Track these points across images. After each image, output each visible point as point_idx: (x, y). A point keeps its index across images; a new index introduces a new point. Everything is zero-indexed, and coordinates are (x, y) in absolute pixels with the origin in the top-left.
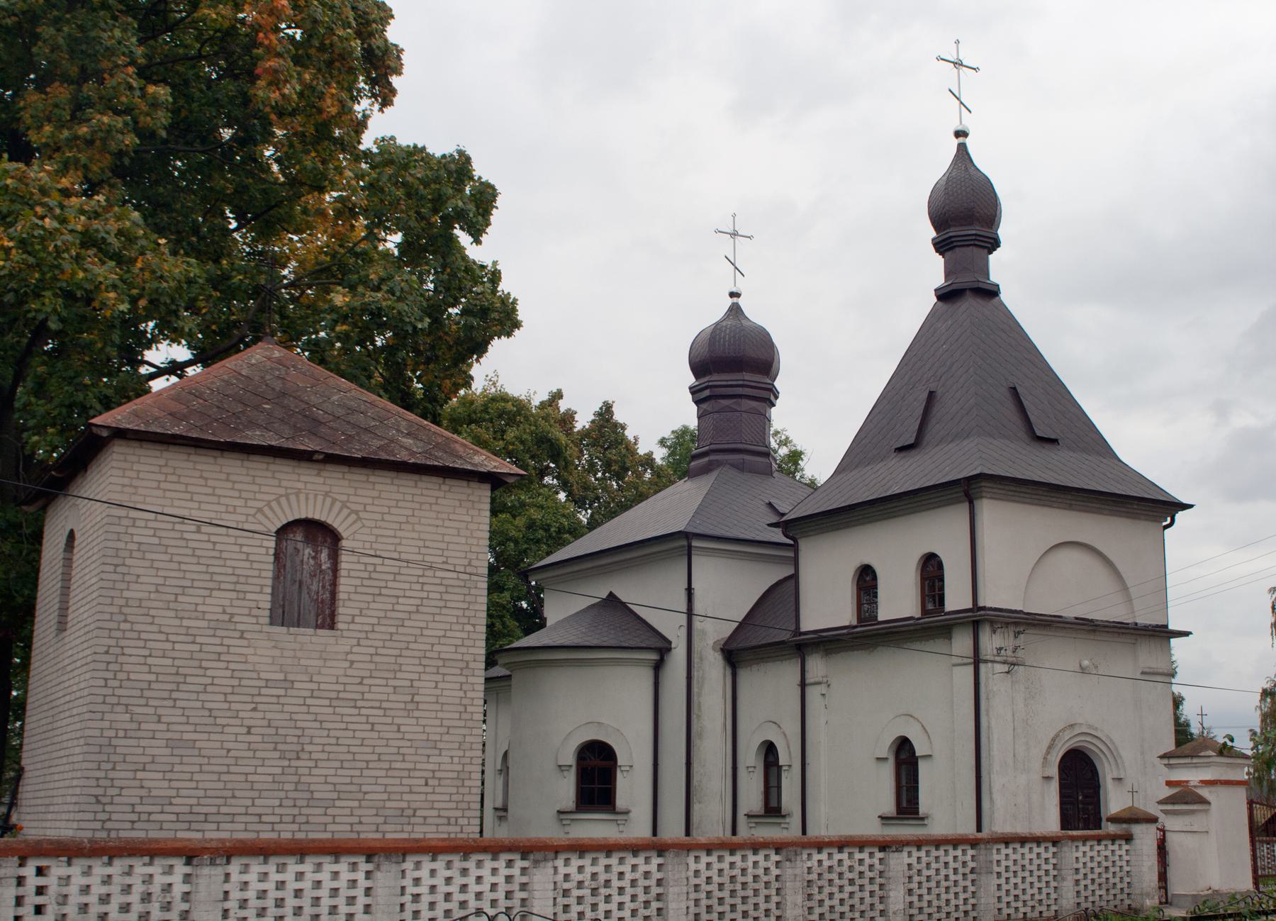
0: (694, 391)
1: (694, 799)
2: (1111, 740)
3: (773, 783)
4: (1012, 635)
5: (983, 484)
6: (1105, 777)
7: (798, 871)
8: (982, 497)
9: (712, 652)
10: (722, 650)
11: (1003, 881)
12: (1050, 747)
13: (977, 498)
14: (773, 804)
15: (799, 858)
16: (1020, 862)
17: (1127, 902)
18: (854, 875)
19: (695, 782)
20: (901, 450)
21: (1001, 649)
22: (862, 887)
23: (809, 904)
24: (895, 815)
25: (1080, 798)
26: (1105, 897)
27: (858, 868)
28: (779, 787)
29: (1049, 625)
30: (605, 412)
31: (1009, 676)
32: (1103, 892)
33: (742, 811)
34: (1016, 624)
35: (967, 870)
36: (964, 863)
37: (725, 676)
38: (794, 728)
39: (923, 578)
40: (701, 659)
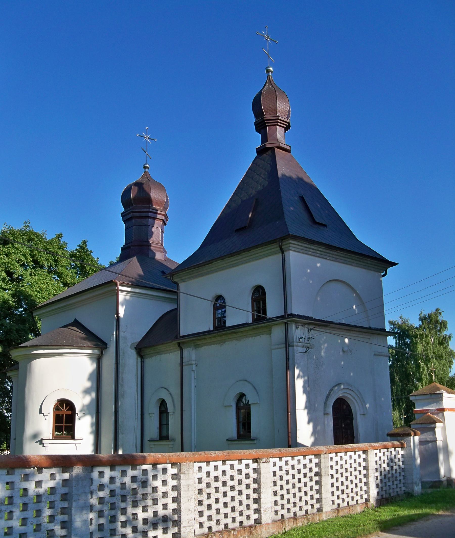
0: (123, 215)
1: (120, 432)
2: (360, 392)
3: (164, 422)
4: (307, 330)
5: (291, 241)
6: (356, 413)
7: (190, 482)
8: (289, 250)
9: (130, 349)
10: (136, 348)
11: (334, 480)
12: (328, 397)
13: (286, 251)
14: (164, 434)
15: (191, 471)
16: (345, 466)
17: (403, 488)
18: (235, 483)
19: (120, 420)
20: (237, 231)
21: (301, 338)
22: (240, 493)
23: (200, 508)
24: (236, 438)
25: (343, 426)
26: (392, 487)
27: (237, 477)
28: (167, 424)
29: (327, 326)
30: (83, 247)
31: (306, 354)
32: (390, 483)
33: (147, 438)
34: (309, 324)
35: (312, 474)
36: (311, 470)
37: (137, 362)
38: (176, 392)
39: (254, 300)
40: (124, 353)
